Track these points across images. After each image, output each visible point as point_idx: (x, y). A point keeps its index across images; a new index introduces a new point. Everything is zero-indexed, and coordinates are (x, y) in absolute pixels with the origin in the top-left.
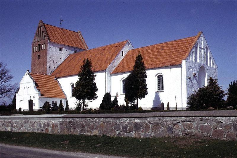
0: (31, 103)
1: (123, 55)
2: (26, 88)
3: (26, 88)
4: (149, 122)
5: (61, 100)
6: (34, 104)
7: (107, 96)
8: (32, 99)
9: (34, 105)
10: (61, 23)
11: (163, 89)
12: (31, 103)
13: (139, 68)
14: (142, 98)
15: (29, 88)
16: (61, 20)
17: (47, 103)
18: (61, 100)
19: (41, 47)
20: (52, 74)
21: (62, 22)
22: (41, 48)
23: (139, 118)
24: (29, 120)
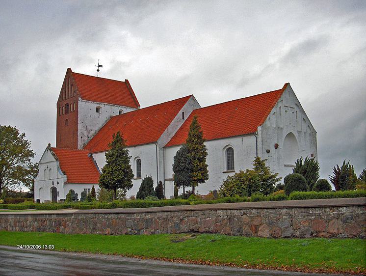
0: (54, 191)
1: (183, 119)
2: (47, 171)
3: (47, 171)
4: (159, 218)
5: (93, 186)
6: (58, 192)
7: (148, 182)
8: (55, 185)
9: (58, 194)
10: (98, 70)
11: (234, 169)
12: (54, 191)
13: (16, 226)
14: (205, 181)
15: (101, 111)
16: (99, 66)
17: (72, 192)
18: (93, 186)
19: (69, 108)
20: (85, 147)
21: (100, 68)
22: (69, 110)
23: (149, 214)
24: (38, 218)
